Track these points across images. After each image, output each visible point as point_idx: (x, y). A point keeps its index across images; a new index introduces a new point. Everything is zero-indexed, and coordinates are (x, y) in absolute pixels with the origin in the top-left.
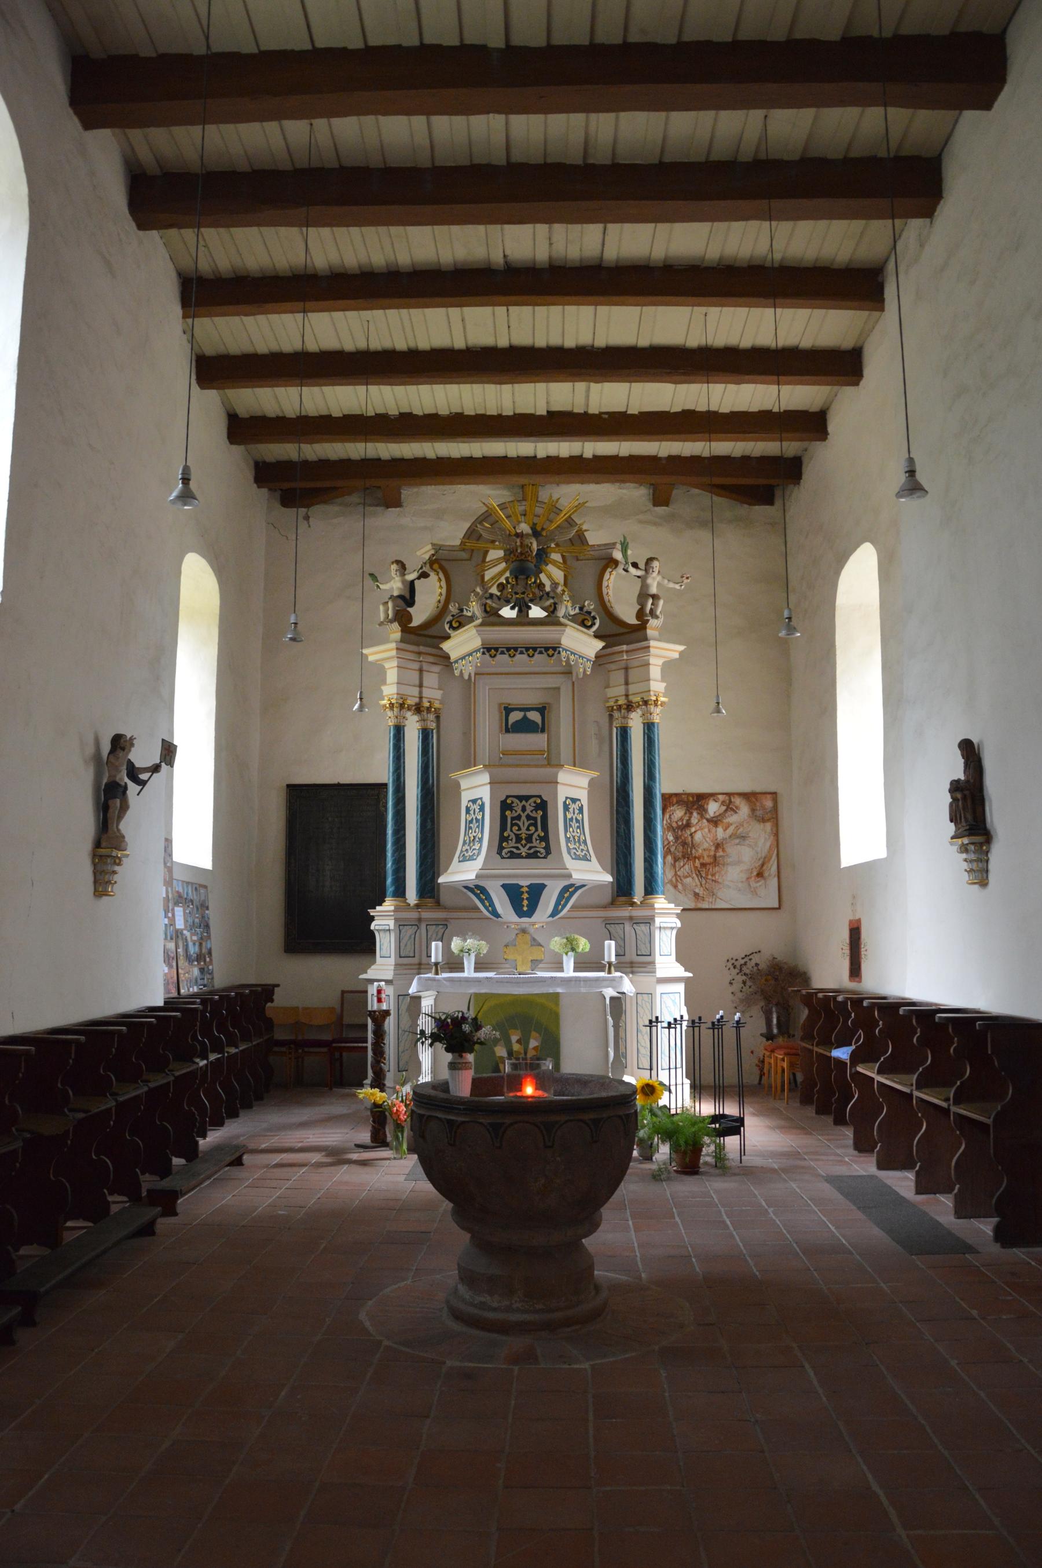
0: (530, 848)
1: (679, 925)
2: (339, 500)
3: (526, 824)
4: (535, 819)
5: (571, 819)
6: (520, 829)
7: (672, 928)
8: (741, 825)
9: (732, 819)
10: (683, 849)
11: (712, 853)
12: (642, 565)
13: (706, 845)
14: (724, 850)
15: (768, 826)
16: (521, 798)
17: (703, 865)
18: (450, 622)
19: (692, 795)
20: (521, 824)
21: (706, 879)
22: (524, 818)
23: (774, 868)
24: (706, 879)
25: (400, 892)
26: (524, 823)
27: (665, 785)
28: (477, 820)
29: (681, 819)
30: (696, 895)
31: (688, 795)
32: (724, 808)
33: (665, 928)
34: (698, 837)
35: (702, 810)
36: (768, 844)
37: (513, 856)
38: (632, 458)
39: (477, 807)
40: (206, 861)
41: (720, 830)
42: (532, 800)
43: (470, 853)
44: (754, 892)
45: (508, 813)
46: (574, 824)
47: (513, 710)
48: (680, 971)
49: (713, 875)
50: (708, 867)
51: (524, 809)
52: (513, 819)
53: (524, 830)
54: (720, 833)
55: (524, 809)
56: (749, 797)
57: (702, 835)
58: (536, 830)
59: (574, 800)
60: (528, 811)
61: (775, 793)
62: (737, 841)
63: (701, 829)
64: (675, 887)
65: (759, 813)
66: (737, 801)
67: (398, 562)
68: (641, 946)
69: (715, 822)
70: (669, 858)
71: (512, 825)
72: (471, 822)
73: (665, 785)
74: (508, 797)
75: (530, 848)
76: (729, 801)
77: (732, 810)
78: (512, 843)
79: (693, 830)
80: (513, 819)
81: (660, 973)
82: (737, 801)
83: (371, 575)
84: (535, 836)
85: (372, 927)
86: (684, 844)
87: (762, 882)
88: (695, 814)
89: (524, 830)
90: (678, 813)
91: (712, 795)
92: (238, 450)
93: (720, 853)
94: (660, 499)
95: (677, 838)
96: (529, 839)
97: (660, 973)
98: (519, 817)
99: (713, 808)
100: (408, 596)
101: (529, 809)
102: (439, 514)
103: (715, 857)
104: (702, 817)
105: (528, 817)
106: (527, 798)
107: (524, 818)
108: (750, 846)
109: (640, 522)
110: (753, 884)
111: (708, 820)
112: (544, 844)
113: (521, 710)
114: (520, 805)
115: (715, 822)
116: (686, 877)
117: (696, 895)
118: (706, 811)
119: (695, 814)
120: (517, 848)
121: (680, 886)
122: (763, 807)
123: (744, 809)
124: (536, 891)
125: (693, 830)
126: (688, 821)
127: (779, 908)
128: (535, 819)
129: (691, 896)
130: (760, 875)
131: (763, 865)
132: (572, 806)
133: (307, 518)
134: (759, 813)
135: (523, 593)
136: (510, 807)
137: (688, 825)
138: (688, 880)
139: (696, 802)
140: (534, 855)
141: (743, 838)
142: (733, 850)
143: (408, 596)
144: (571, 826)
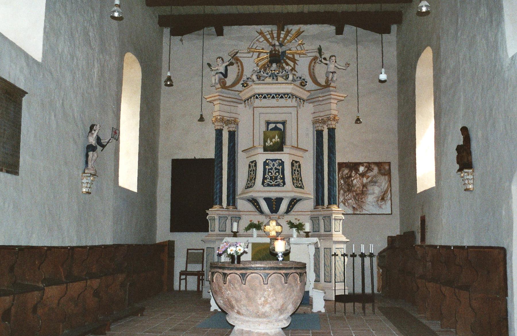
0: (276, 182)
1: (344, 218)
2: (196, 32)
3: (275, 172)
4: (279, 170)
5: (295, 170)
6: (272, 174)
7: (340, 220)
8: (375, 176)
9: (370, 174)
10: (349, 187)
11: (361, 189)
12: (328, 59)
13: (358, 186)
14: (366, 188)
15: (387, 177)
16: (272, 160)
17: (357, 194)
18: (243, 84)
19: (353, 163)
20: (272, 172)
21: (358, 201)
22: (274, 169)
23: (389, 196)
24: (358, 201)
25: (221, 203)
26: (274, 171)
27: (339, 159)
28: (254, 170)
29: (347, 174)
30: (354, 208)
31: (351, 163)
32: (366, 169)
33: (337, 219)
34: (355, 182)
35: (357, 170)
36: (386, 185)
37: (269, 185)
38: (326, 13)
39: (253, 164)
40: (134, 188)
41: (365, 179)
42: (278, 161)
43: (250, 185)
44: (380, 207)
45: (267, 167)
46: (296, 173)
47: (271, 123)
48: (344, 239)
49: (362, 199)
50: (360, 195)
51: (274, 165)
52: (269, 169)
53: (273, 174)
54: (365, 180)
55: (274, 165)
56: (379, 164)
57: (356, 181)
58: (279, 174)
59: (296, 162)
60: (276, 166)
61: (390, 163)
62: (372, 184)
63: (356, 178)
64: (344, 204)
65: (383, 171)
66: (373, 166)
67: (219, 58)
68: (326, 227)
69: (363, 175)
70: (342, 192)
71: (269, 172)
72: (251, 171)
73: (339, 159)
74: (267, 160)
75: (276, 182)
76: (369, 166)
77: (370, 170)
78: (268, 180)
79: (353, 179)
80: (269, 169)
81: (335, 239)
82: (373, 166)
83: (209, 65)
84: (279, 177)
85: (207, 218)
86: (349, 185)
87: (384, 202)
88: (354, 172)
89: (273, 174)
90: (346, 171)
91: (361, 164)
92: (150, 10)
93: (365, 189)
94: (339, 31)
95: (345, 182)
96: (276, 178)
97: (335, 239)
98: (272, 169)
99: (362, 169)
100: (224, 72)
101: (276, 165)
102: (240, 39)
103: (362, 191)
104: (356, 173)
105: (276, 169)
106: (275, 160)
107: (274, 169)
108: (378, 186)
109: (330, 42)
110: (379, 203)
111: (359, 174)
112: (282, 181)
113: (274, 123)
114: (272, 163)
115: (363, 175)
116: (349, 200)
117: (354, 208)
118: (359, 170)
119: (354, 172)
120: (271, 182)
121: (346, 204)
122: (384, 168)
123: (376, 170)
124: (279, 200)
125: (353, 179)
126: (351, 175)
127: (391, 214)
128: (279, 170)
129: (351, 208)
130: (383, 199)
131: (384, 194)
132: (295, 164)
133: (181, 40)
134: (383, 171)
135: (274, 70)
136: (268, 164)
137: (351, 176)
138: (351, 201)
139: (354, 166)
140: (278, 185)
141: (376, 182)
142: (370, 188)
143: (224, 72)
144: (295, 173)
